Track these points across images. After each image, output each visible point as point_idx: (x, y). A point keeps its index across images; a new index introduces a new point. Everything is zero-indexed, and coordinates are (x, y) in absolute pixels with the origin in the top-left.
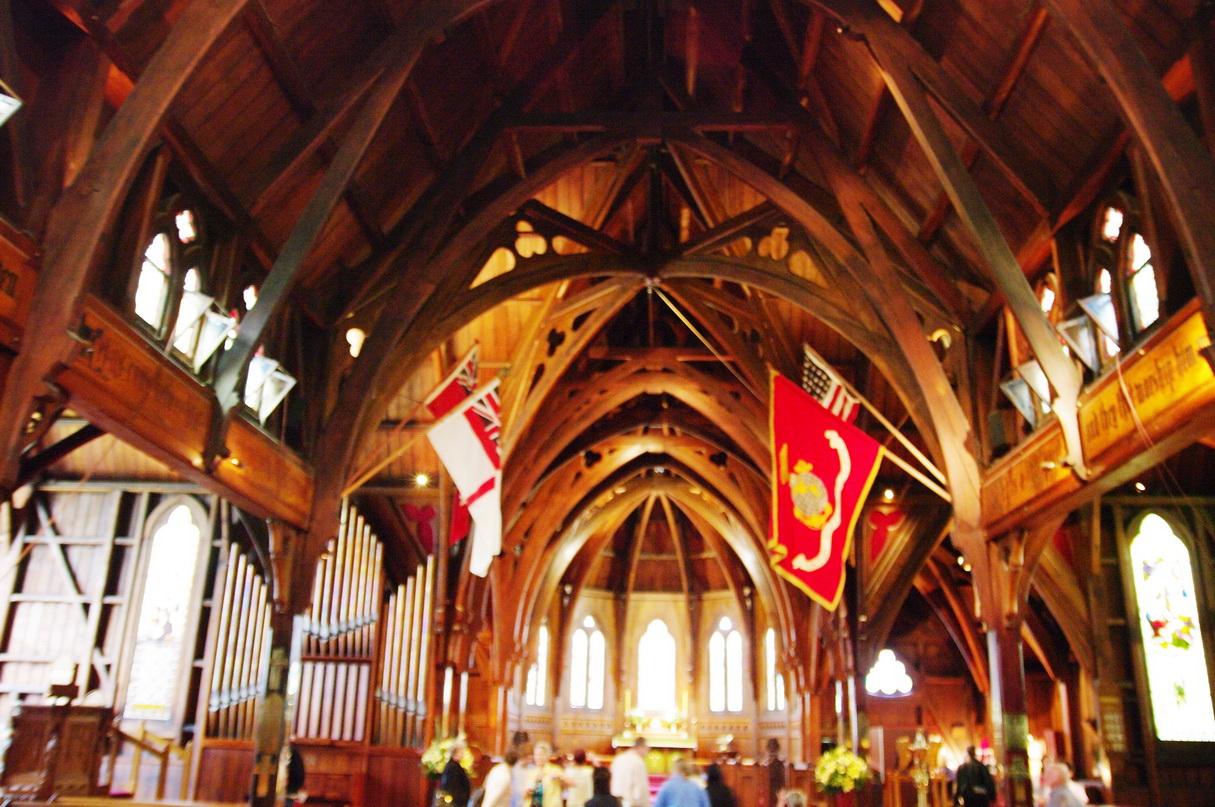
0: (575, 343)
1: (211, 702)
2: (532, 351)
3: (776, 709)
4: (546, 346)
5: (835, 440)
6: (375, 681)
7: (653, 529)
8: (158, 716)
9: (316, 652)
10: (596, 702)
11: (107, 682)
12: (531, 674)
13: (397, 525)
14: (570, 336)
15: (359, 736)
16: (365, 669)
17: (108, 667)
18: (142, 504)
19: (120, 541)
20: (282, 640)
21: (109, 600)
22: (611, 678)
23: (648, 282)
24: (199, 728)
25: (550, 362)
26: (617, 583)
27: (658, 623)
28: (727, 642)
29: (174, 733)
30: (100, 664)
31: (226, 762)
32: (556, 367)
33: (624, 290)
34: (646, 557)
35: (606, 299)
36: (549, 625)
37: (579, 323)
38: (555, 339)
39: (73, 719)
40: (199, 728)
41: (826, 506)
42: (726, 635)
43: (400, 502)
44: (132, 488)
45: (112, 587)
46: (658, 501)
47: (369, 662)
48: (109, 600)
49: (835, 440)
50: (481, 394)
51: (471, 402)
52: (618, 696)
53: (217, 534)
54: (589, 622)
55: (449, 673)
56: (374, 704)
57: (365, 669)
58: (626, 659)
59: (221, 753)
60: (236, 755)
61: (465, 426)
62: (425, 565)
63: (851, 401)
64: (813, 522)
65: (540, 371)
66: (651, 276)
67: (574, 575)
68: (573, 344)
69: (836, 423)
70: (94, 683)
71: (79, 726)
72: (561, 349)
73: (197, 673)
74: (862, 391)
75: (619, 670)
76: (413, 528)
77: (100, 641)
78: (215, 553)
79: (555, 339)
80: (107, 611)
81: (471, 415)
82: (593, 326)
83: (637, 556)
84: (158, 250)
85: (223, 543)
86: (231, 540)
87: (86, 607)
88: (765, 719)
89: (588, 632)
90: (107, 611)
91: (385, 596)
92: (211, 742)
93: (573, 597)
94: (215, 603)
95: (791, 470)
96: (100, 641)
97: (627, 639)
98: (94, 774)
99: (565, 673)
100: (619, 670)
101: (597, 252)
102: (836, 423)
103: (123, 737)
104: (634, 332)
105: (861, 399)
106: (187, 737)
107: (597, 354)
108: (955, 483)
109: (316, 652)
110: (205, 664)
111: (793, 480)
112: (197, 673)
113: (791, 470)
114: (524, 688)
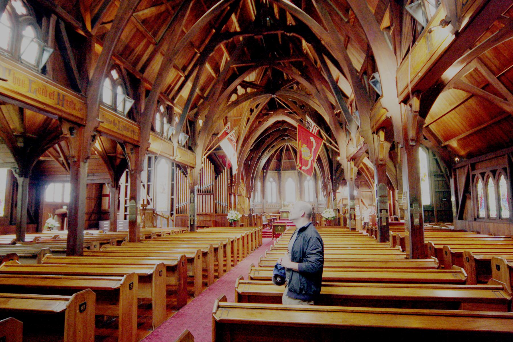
0: (256, 112)
1: (176, 206)
2: (246, 114)
3: (272, 202)
4: (250, 113)
5: (312, 139)
6: (215, 199)
7: (287, 153)
8: (164, 210)
9: (200, 192)
10: (274, 201)
11: (151, 203)
12: (256, 194)
13: (217, 160)
14: (255, 110)
15: (212, 212)
16: (212, 196)
17: (151, 199)
18: (153, 159)
19: (149, 169)
20: (192, 192)
21: (149, 183)
22: (278, 194)
23: (273, 96)
24: (174, 212)
25: (251, 117)
26: (278, 168)
27: (290, 179)
28: (309, 183)
29: (169, 213)
30: (149, 198)
31: (182, 219)
32: (252, 118)
33: (267, 98)
34: (286, 161)
35: (263, 100)
36: (261, 181)
37: (257, 106)
38: (252, 111)
39: (146, 211)
40: (174, 212)
41: (309, 154)
42: (309, 181)
43: (217, 155)
44: (150, 155)
45: (149, 181)
46: (287, 146)
47: (213, 194)
48: (149, 183)
49: (312, 139)
50: (230, 134)
51: (229, 136)
52: (280, 199)
53: (173, 166)
54: (271, 179)
55: (233, 195)
56: (215, 204)
57: (212, 196)
58: (281, 189)
59: (180, 217)
60: (184, 217)
61: (227, 141)
62: (225, 169)
63: (317, 129)
64: (307, 158)
65: (249, 119)
66: (274, 95)
67: (266, 167)
68: (256, 112)
69: (313, 135)
70: (148, 203)
71: (148, 213)
72: (253, 114)
73: (172, 199)
74: (320, 127)
75: (280, 191)
76: (221, 160)
77: (148, 193)
78: (173, 170)
79: (252, 111)
80: (149, 186)
81: (228, 139)
82: (260, 107)
83: (283, 161)
84: (158, 116)
85: (175, 168)
86: (176, 167)
87: (144, 186)
88: (319, 203)
89: (271, 182)
90: (149, 186)
91: (216, 178)
92: (177, 215)
93: (266, 173)
94: (174, 182)
95: (301, 147)
96: (148, 193)
97: (282, 183)
98: (153, 223)
99: (265, 193)
100: (280, 191)
101: (261, 89)
102: (313, 135)
103: (157, 215)
104: (273, 107)
105: (319, 128)
106: (172, 214)
107: (263, 112)
108: (340, 148)
109: (200, 192)
110: (174, 197)
111: (302, 149)
112: (172, 199)
113: (301, 147)
114: (254, 198)
